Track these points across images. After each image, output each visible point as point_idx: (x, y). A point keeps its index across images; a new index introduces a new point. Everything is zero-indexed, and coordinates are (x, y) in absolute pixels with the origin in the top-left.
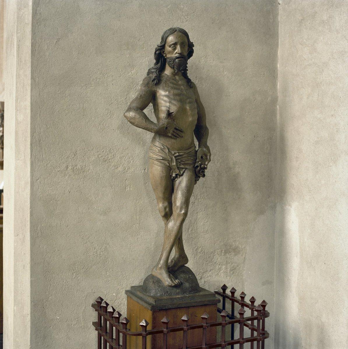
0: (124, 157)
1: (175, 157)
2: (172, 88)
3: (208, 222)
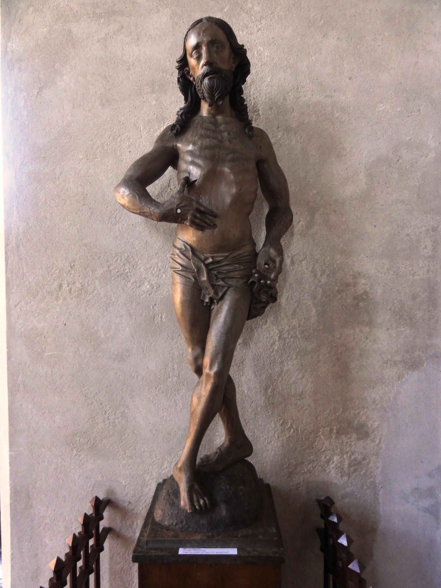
0: (152, 269)
1: (207, 266)
2: (201, 136)
3: (304, 379)
